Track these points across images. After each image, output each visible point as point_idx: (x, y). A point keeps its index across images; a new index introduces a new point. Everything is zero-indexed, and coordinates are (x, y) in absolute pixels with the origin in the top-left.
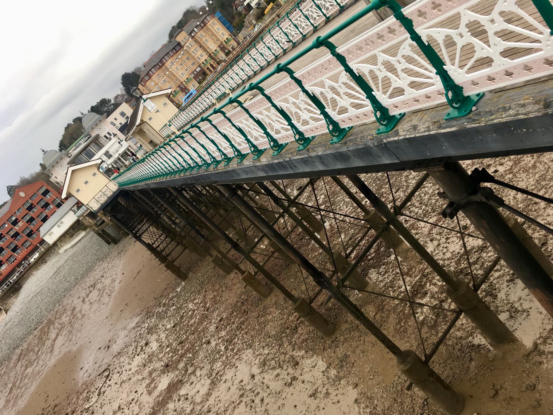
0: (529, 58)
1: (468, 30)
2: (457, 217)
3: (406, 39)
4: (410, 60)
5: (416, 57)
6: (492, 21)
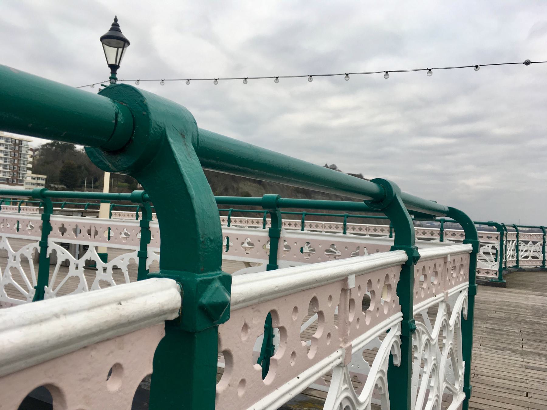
0: (378, 325)
1: (97, 272)
2: (476, 223)
3: (37, 241)
4: (24, 261)
5: (31, 262)
6: (105, 270)
